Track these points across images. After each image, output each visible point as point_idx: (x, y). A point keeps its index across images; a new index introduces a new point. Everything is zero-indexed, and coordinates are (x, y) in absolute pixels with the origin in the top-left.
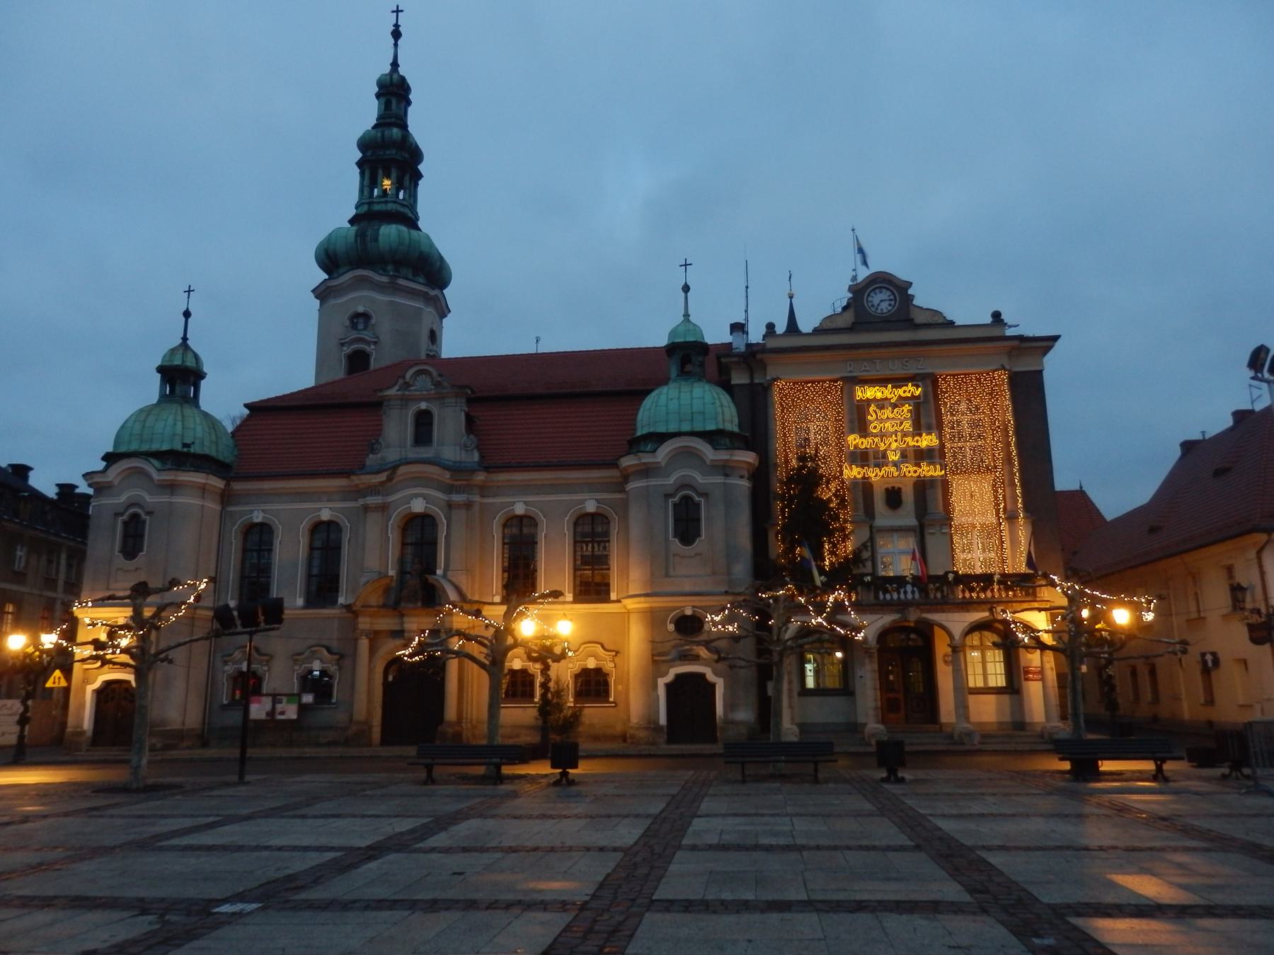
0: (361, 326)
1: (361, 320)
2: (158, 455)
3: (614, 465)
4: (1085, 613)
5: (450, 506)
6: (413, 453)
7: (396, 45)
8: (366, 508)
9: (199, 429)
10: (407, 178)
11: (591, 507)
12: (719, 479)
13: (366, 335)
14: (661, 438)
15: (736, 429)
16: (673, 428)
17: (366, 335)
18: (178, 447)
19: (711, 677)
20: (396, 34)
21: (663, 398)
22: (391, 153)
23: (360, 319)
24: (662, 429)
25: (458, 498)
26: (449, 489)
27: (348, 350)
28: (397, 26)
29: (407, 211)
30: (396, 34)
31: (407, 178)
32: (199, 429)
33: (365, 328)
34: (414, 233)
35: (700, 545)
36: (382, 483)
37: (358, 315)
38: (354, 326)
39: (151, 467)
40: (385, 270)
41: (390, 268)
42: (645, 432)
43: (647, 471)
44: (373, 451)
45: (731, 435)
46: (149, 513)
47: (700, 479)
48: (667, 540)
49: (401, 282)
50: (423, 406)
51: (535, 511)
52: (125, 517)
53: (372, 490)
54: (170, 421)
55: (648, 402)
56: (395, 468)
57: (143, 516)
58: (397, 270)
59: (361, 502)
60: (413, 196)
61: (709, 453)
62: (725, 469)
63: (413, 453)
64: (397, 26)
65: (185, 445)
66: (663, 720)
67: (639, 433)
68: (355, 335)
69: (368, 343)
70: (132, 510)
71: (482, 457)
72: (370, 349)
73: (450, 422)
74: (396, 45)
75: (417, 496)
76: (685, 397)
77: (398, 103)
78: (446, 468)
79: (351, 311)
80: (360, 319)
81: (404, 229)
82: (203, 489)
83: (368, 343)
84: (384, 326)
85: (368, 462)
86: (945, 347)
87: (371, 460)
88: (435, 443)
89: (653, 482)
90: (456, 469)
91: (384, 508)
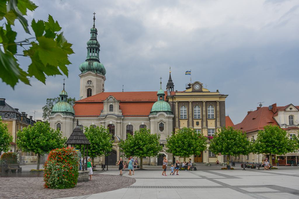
0: (89, 83)
1: (90, 82)
2: (62, 112)
3: (148, 116)
4: (161, 160)
5: (117, 123)
6: (110, 113)
7: (94, 21)
8: (101, 123)
9: (69, 107)
10: (97, 51)
11: (143, 124)
12: (168, 120)
13: (91, 85)
14: (157, 112)
15: (170, 111)
16: (159, 110)
17: (91, 85)
18: (66, 111)
19: (165, 154)
20: (94, 19)
21: (157, 104)
22: (94, 46)
23: (89, 82)
24: (157, 110)
25: (119, 121)
26: (117, 120)
27: (88, 88)
28: (94, 17)
29: (97, 58)
30: (94, 19)
31: (97, 51)
32: (69, 107)
33: (91, 84)
34: (100, 63)
35: (164, 131)
36: (104, 118)
37: (89, 81)
38: (88, 83)
39: (62, 115)
40: (94, 72)
41: (95, 71)
42: (154, 111)
43: (154, 118)
44: (102, 112)
45: (170, 112)
46: (61, 123)
47: (164, 120)
48: (158, 130)
49: (98, 74)
50: (111, 104)
51: (132, 124)
52: (160, 123)
53: (102, 119)
54: (64, 106)
55: (155, 105)
56: (107, 116)
57: (61, 124)
58: (97, 72)
59: (100, 122)
60: (98, 54)
61: (166, 115)
62: (169, 118)
63: (110, 113)
64: (94, 17)
65: (67, 110)
66: (157, 162)
67: (152, 111)
68: (88, 85)
69: (91, 87)
70: (58, 122)
71: (122, 114)
72: (92, 88)
73: (116, 106)
74: (94, 21)
75: (111, 121)
76: (161, 104)
77: (95, 34)
78: (116, 116)
79: (87, 80)
80: (89, 82)
81: (98, 63)
82: (71, 118)
83: (91, 87)
84: (94, 83)
85: (101, 114)
86: (194, 179)
87: (102, 114)
88: (114, 111)
89: (156, 120)
90: (118, 116)
91: (105, 123)
